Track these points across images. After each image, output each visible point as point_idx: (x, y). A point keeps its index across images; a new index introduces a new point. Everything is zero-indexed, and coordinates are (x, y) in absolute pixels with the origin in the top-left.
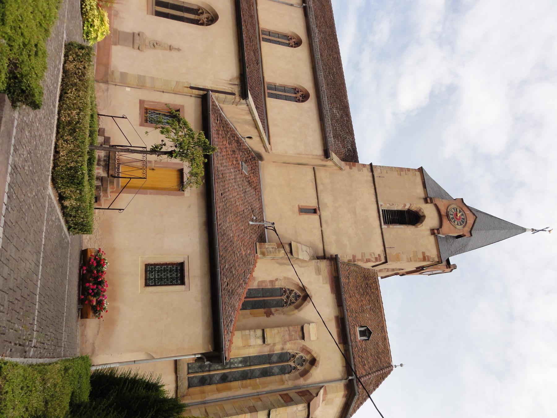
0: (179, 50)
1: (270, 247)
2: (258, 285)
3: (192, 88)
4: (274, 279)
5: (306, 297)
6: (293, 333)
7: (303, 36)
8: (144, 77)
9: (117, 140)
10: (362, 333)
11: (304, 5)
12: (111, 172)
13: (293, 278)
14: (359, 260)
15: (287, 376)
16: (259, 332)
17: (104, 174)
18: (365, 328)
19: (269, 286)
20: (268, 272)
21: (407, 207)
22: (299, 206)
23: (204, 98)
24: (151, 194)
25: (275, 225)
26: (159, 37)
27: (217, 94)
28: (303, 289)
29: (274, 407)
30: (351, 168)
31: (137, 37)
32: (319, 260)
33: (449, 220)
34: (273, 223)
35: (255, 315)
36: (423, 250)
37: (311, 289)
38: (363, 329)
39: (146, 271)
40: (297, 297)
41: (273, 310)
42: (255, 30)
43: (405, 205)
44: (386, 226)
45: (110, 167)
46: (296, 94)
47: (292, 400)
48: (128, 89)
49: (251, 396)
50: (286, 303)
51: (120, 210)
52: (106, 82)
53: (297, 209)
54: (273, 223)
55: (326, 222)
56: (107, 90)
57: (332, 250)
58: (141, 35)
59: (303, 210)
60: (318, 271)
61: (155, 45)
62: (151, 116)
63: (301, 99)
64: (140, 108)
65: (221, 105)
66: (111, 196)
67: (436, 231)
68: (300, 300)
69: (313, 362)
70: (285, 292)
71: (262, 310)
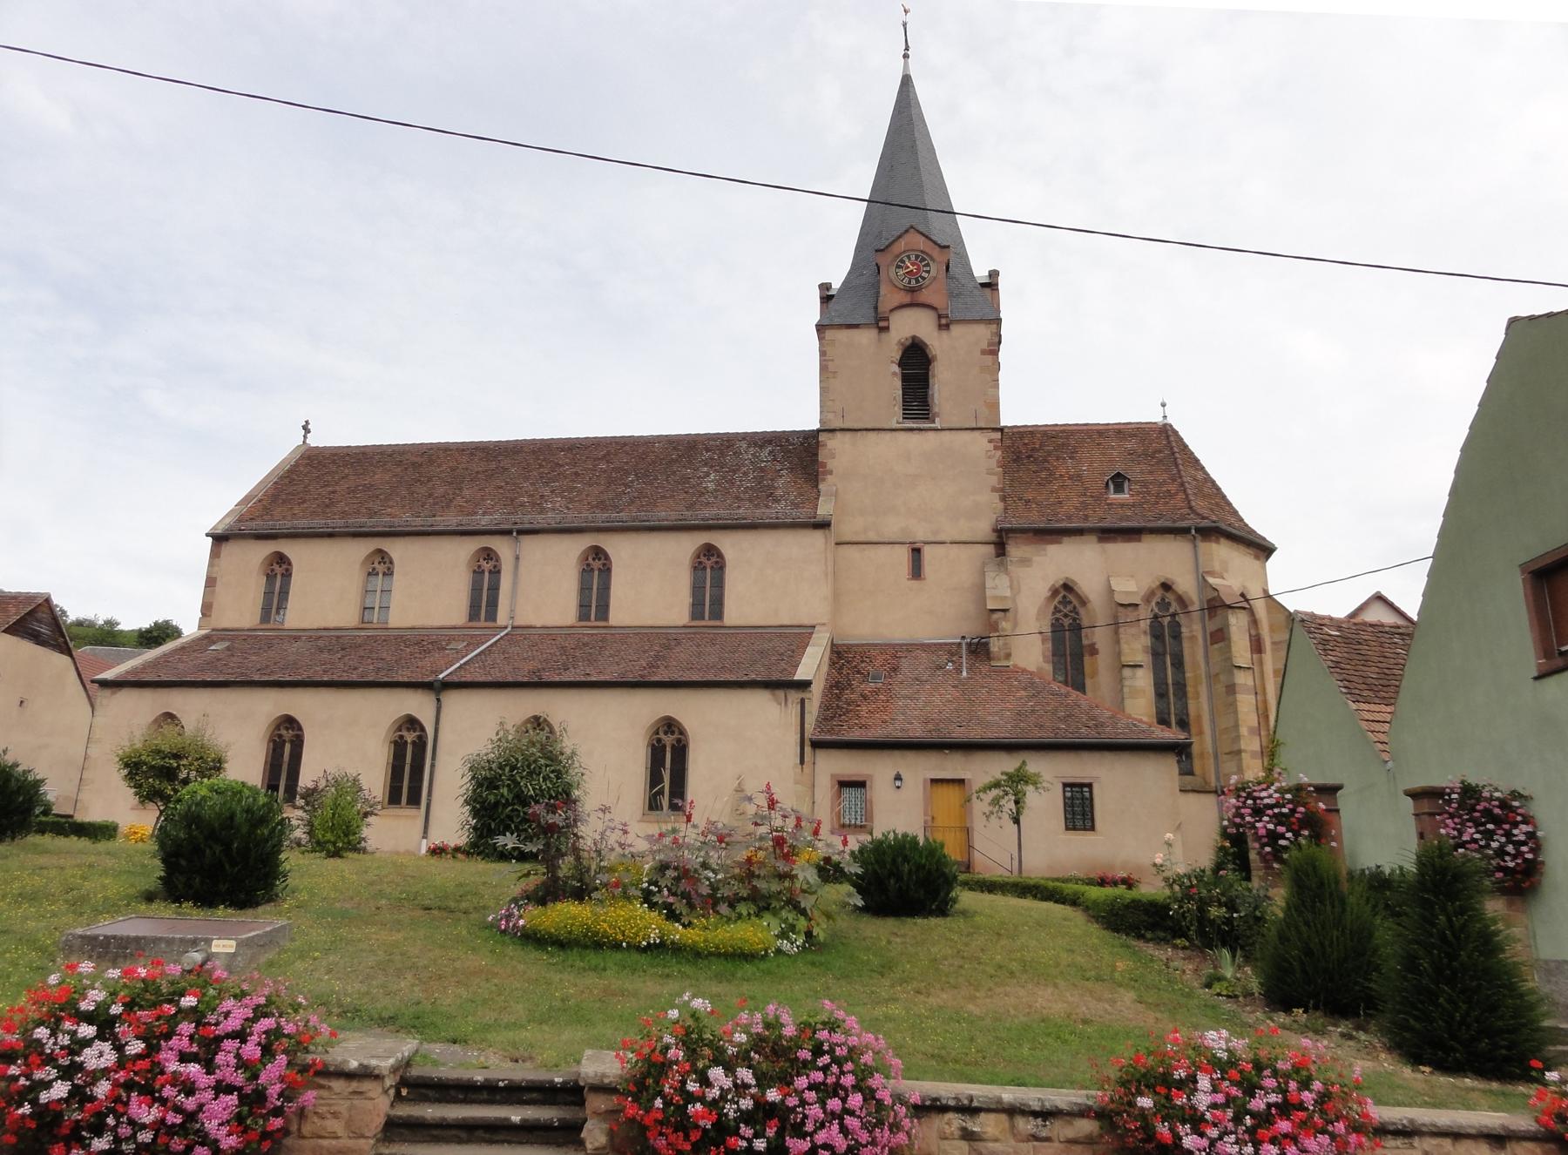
3: (802, 762)
5: (1068, 587)
15: (1184, 629)
16: (1127, 672)
19: (1049, 645)
21: (896, 369)
29: (1229, 659)
30: (831, 473)
33: (920, 288)
35: (1095, 674)
39: (1074, 829)
40: (1065, 602)
41: (1085, 642)
43: (894, 374)
47: (1220, 630)
49: (1210, 687)
53: (915, 583)
57: (983, 527)
59: (917, 571)
60: (1025, 562)
63: (714, 559)
68: (1071, 597)
69: (1166, 587)
71: (1087, 659)
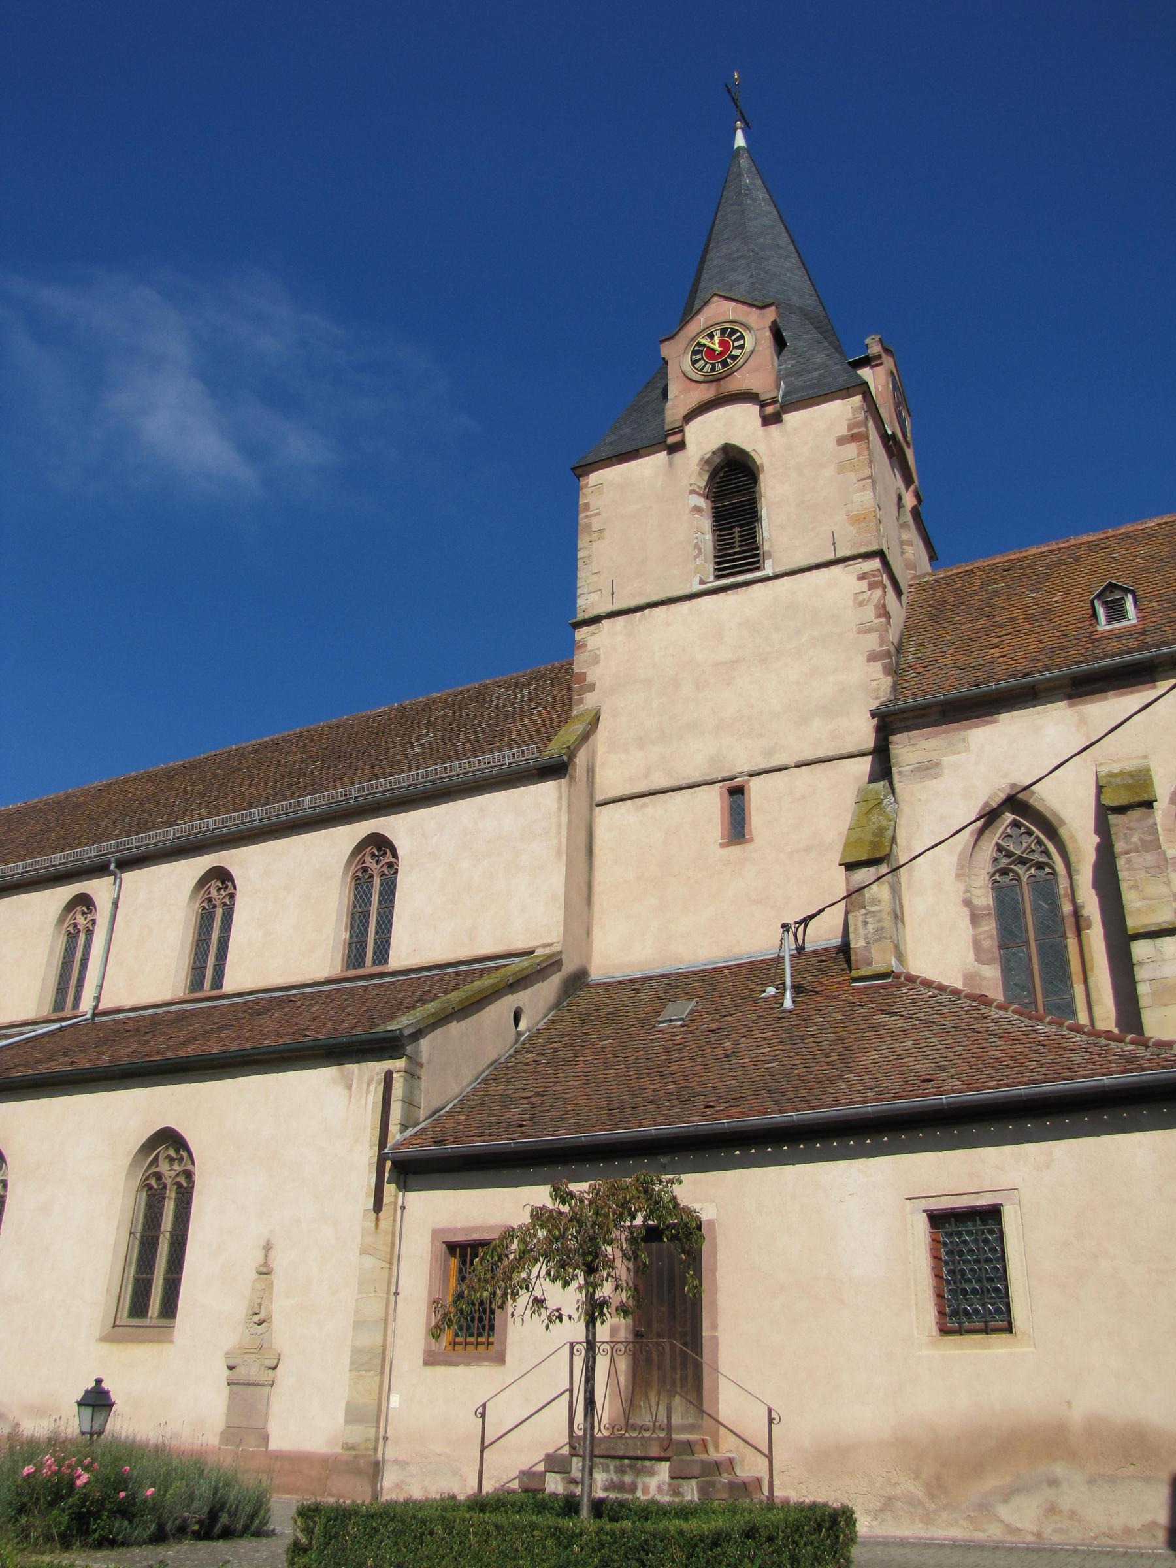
0: (268, 1248)
1: (862, 931)
2: (989, 962)
3: (378, 1206)
4: (966, 912)
5: (1017, 804)
6: (1135, 839)
7: (65, 893)
8: (355, 1351)
9: (552, 1431)
10: (1116, 612)
11: (112, 866)
12: (654, 1451)
13: (959, 848)
14: (882, 642)
17: (664, 1469)
18: (1097, 603)
19: (990, 926)
20: (941, 936)
21: (702, 502)
22: (722, 846)
23: (408, 1169)
24: (715, 1327)
25: (790, 920)
26: (236, 1307)
27: (393, 1128)
28: (990, 817)
30: (592, 687)
31: (242, 1373)
32: (895, 770)
34: (785, 927)
36: (831, 443)
37: (988, 788)
38: (1101, 612)
39: (960, 1332)
42: (193, 1013)
43: (697, 509)
44: (768, 563)
45: (639, 1453)
46: (372, 876)
48: (395, 1401)
50: (1040, 866)
51: (771, 1420)
52: (376, 1469)
53: (735, 851)
54: (785, 927)
55: (769, 753)
56: (400, 1464)
58: (232, 1363)
59: (737, 827)
60: (929, 769)
61: (260, 1319)
62: (470, 1316)
64: (447, 1363)
65: (422, 1114)
66: (727, 1447)
67: (770, 410)
70: (1004, 872)
